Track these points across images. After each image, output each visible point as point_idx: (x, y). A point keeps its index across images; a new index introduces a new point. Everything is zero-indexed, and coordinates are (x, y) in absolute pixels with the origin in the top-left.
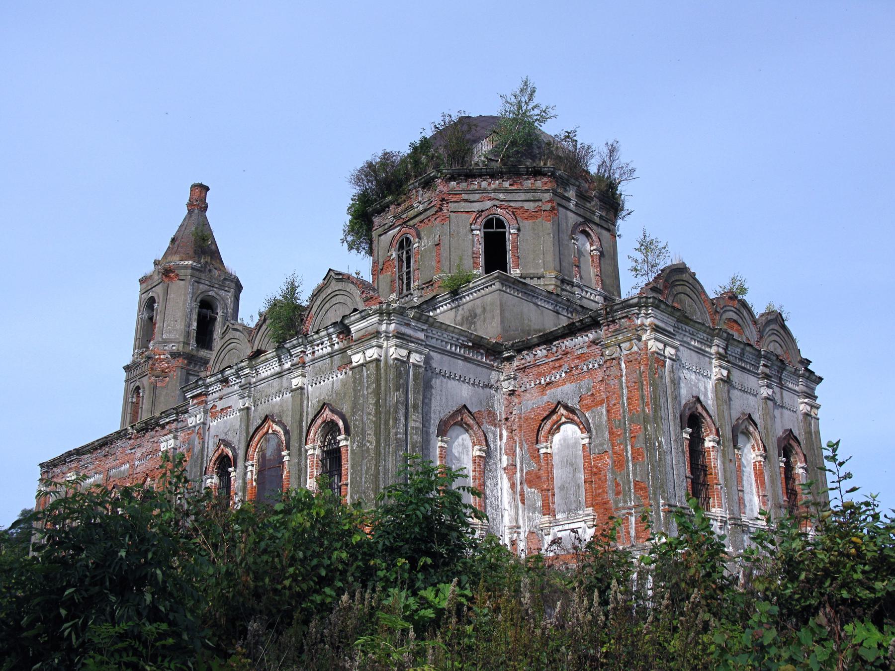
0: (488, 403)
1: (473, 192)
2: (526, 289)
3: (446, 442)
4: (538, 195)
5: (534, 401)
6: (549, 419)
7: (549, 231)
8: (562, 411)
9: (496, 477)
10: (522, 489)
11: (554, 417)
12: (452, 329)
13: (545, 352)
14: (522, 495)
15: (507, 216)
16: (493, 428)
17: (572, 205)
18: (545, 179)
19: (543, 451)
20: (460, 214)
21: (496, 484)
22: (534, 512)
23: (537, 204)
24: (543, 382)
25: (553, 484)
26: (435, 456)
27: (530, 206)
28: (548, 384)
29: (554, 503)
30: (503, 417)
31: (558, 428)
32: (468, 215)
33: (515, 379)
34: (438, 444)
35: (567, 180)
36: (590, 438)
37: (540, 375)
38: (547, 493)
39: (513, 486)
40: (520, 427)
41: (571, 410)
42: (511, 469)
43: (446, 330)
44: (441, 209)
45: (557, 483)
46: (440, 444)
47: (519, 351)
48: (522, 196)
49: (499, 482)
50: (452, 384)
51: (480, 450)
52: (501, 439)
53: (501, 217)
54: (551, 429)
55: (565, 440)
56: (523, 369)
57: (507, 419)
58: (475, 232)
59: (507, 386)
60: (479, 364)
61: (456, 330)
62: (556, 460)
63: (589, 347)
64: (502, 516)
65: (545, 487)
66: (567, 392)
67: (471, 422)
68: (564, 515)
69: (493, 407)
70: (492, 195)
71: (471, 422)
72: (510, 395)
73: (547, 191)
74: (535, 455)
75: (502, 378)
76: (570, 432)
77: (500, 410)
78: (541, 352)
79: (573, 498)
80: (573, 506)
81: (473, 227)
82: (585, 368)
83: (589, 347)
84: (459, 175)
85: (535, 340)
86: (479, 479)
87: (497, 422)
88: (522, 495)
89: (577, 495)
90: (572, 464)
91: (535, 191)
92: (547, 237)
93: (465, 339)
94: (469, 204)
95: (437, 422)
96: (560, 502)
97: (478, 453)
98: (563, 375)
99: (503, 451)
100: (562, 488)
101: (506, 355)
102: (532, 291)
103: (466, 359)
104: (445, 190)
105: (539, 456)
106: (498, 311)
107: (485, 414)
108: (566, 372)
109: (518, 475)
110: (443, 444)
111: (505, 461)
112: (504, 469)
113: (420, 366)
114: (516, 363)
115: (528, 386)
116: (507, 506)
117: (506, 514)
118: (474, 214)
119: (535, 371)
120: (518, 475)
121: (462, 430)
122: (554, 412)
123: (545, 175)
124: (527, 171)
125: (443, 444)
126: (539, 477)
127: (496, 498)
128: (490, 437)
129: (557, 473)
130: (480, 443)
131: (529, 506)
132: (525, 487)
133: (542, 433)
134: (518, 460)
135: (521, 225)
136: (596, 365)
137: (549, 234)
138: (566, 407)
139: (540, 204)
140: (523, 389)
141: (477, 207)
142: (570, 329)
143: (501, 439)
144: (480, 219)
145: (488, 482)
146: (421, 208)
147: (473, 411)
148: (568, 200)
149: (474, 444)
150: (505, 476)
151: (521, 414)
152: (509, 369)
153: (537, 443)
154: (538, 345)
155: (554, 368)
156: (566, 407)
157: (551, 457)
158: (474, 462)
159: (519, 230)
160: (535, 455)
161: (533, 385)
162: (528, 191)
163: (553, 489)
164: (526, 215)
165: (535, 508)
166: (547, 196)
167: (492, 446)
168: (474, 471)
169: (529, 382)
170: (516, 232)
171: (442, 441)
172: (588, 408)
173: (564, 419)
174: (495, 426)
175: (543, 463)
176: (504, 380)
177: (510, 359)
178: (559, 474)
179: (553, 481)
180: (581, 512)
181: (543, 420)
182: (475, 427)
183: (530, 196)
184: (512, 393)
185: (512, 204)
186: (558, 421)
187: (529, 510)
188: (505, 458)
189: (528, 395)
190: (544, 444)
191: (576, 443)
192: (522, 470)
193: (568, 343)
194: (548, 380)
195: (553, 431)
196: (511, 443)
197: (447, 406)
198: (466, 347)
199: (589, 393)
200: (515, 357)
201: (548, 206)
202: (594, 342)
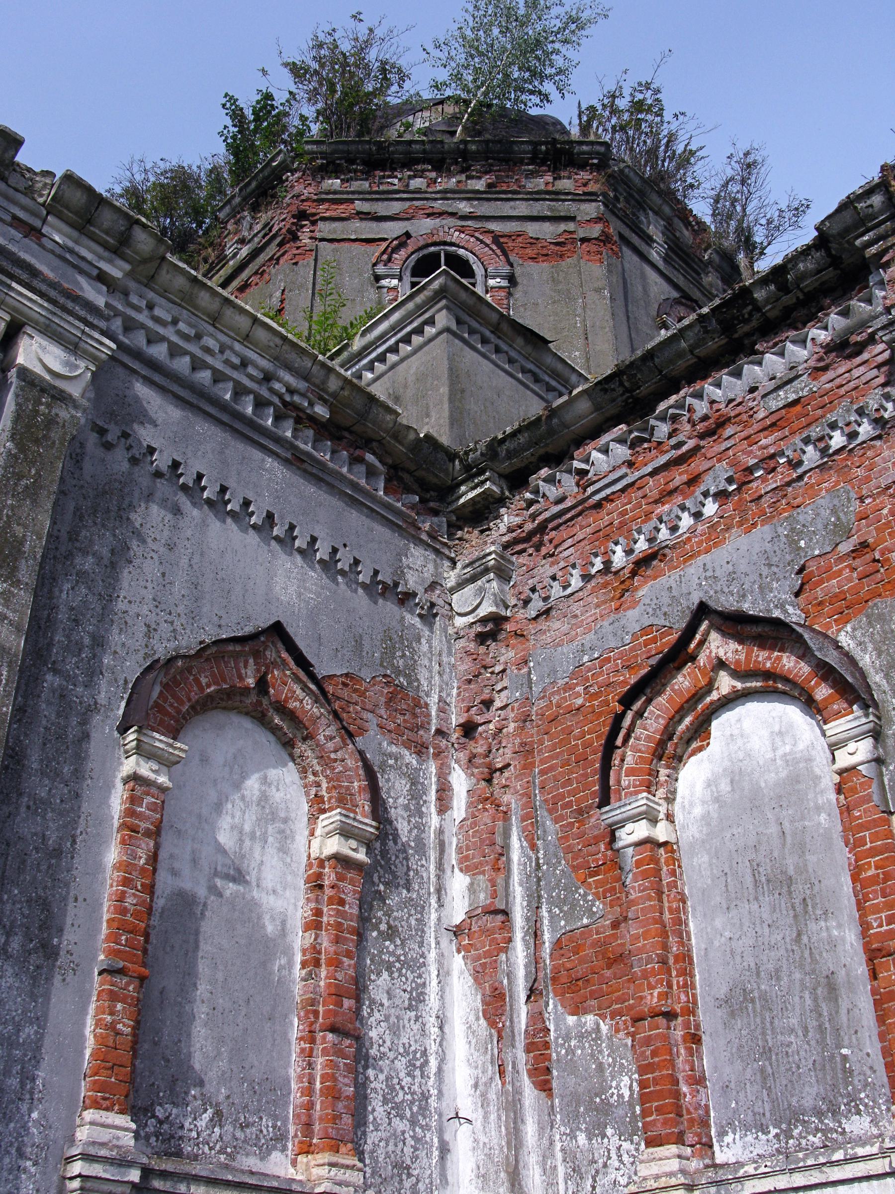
0: (389, 653)
1: (387, 196)
2: (539, 364)
3: (167, 763)
4: (565, 207)
5: (584, 637)
6: (657, 697)
7: (600, 284)
8: (718, 646)
9: (417, 965)
10: (537, 1019)
11: (683, 681)
12: (243, 323)
13: (621, 452)
14: (538, 1046)
15: (478, 248)
16: (410, 758)
17: (654, 255)
18: (584, 175)
19: (639, 830)
20: (346, 245)
21: (418, 998)
22: (597, 1131)
23: (563, 227)
24: (619, 558)
25: (688, 987)
26: (103, 820)
27: (547, 231)
28: (643, 563)
29: (698, 1081)
30: (455, 719)
31: (700, 731)
32: (369, 248)
33: (503, 574)
34: (122, 766)
35: (641, 192)
36: (877, 735)
37: (604, 537)
38: (663, 1030)
39: (495, 1004)
40: (526, 751)
41: (769, 632)
42: (485, 932)
43: (215, 319)
44: (295, 238)
45: (709, 981)
46: (129, 765)
47: (518, 480)
48: (522, 208)
49: (433, 987)
50: (222, 535)
51: (345, 832)
52: (445, 804)
53: (461, 252)
54: (668, 734)
55: (735, 776)
56: (531, 539)
57: (469, 729)
58: (384, 282)
59: (471, 603)
60: (355, 499)
61: (261, 335)
62: (697, 872)
63: (818, 371)
64: (444, 1149)
65: (652, 998)
66: (742, 565)
67: (305, 704)
68: (762, 1144)
69: (410, 672)
70: (438, 205)
71: (305, 704)
72: (482, 638)
73: (590, 197)
74: (598, 860)
75: (451, 578)
76: (761, 735)
77: (442, 691)
78: (605, 457)
79: (803, 1051)
80: (809, 1094)
81: (381, 269)
82: (811, 455)
83: (818, 371)
84: (352, 161)
85: (584, 405)
86: (335, 963)
87: (427, 735)
88: (538, 1046)
89: (828, 1033)
90: (782, 883)
91: (556, 195)
92: (592, 296)
93: (302, 385)
94: (374, 224)
95: (132, 669)
96: (730, 1072)
97: (334, 845)
98: (710, 508)
99: (452, 857)
100: (738, 1002)
101: (468, 495)
102: (555, 375)
103: (297, 461)
104: (308, 192)
105: (615, 863)
106: (444, 390)
107: (378, 694)
108: (721, 496)
109: (520, 953)
110: (146, 769)
111: (459, 895)
112: (457, 931)
113: (61, 397)
114: (507, 519)
115: (556, 591)
116: (464, 1099)
117: (462, 1140)
118: (384, 245)
119: (584, 528)
120: (520, 953)
121: (263, 737)
122: (678, 655)
123: (583, 165)
124: (535, 152)
125: (146, 769)
126: (618, 959)
127: (417, 1063)
128: (396, 790)
129: (701, 931)
130: (344, 800)
131: (575, 1099)
132: (552, 1005)
133: (630, 757)
134: (518, 892)
135: (518, 271)
136: (865, 429)
137: (598, 290)
138: (736, 624)
139: (571, 226)
140: (537, 605)
141: (393, 229)
142: (727, 328)
143: (444, 805)
144: (403, 253)
145: (379, 986)
146: (245, 251)
147: (321, 671)
148: (649, 240)
149: (318, 806)
150: (458, 962)
151: (527, 700)
152: (487, 544)
153: (605, 800)
154: (595, 433)
155: (667, 494)
156: (736, 624)
157: (674, 860)
158: (316, 884)
159: (512, 279)
160: (598, 860)
161: (576, 582)
162: (536, 196)
163: (690, 1010)
164: (530, 252)
165: (605, 1109)
166: (591, 209)
167: (403, 827)
168: (314, 925)
169: (564, 574)
170: (505, 283)
171: (141, 750)
172: (847, 607)
173: (725, 683)
174: (420, 750)
175: (635, 886)
176: (461, 585)
177: (481, 514)
178: (716, 936)
179: (687, 972)
180: (857, 1125)
181: (627, 700)
182: (326, 731)
183: (539, 208)
184: (492, 629)
185: (493, 226)
186: (697, 696)
187: (572, 1119)
188: (458, 884)
189: (557, 625)
190: (642, 800)
191: (798, 777)
192: (536, 934)
193: (722, 390)
194: (642, 545)
195: (673, 749)
196: (486, 818)
197: (193, 616)
198: (303, 419)
199: (845, 547)
200: (501, 501)
201: (595, 231)
202: (843, 348)
